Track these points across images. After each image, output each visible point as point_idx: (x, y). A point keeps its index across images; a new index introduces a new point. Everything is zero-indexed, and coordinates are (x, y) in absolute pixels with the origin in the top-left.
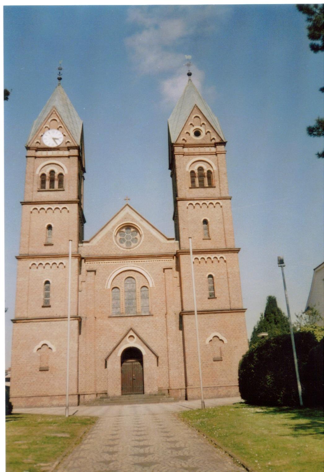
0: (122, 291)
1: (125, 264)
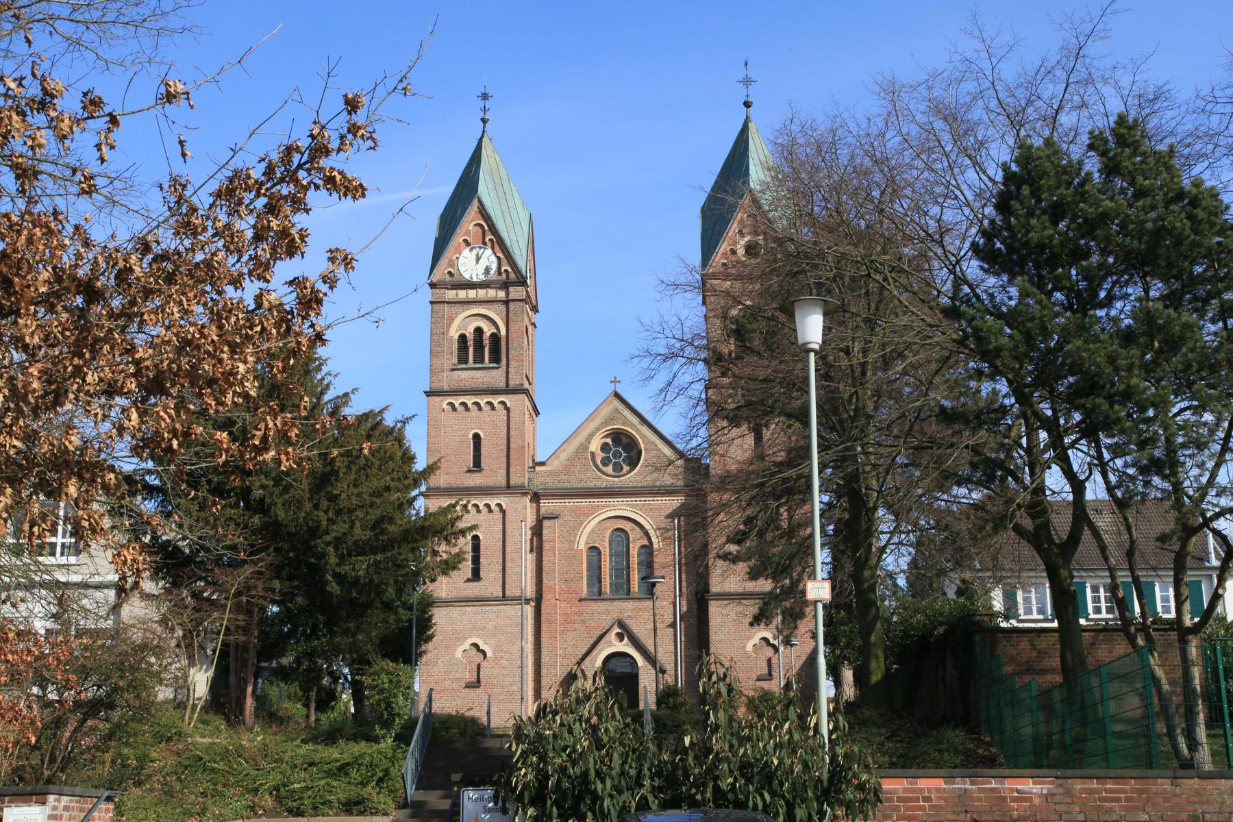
1: (609, 506)
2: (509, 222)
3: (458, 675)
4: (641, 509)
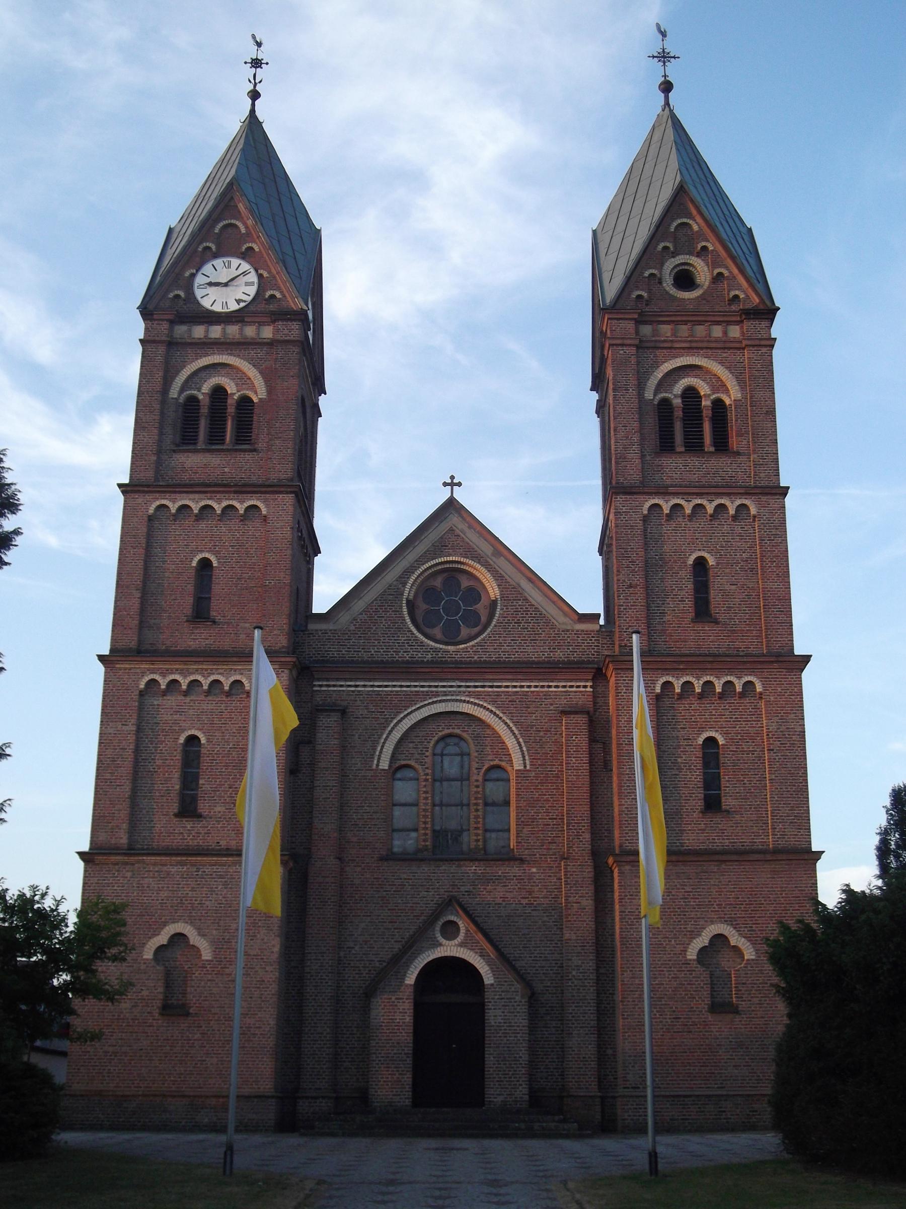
0: (426, 780)
1: (437, 694)
4: (493, 702)
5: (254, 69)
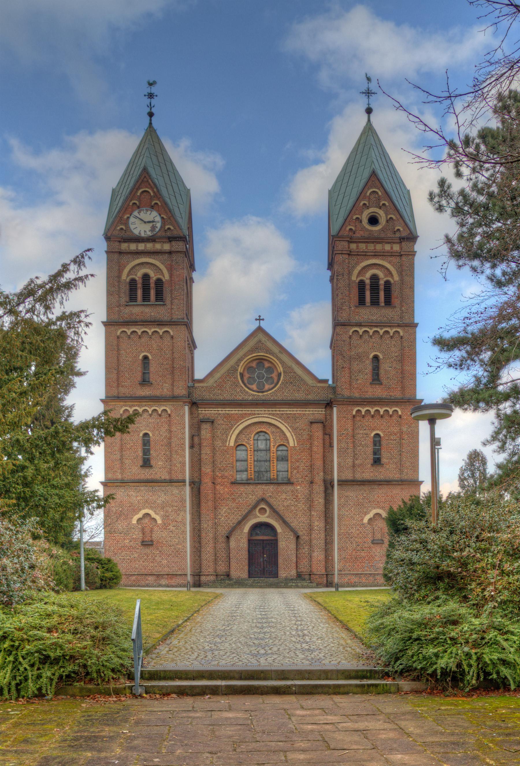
1: (255, 414)
2: (171, 192)
3: (134, 536)
4: (280, 418)
5: (149, 99)
